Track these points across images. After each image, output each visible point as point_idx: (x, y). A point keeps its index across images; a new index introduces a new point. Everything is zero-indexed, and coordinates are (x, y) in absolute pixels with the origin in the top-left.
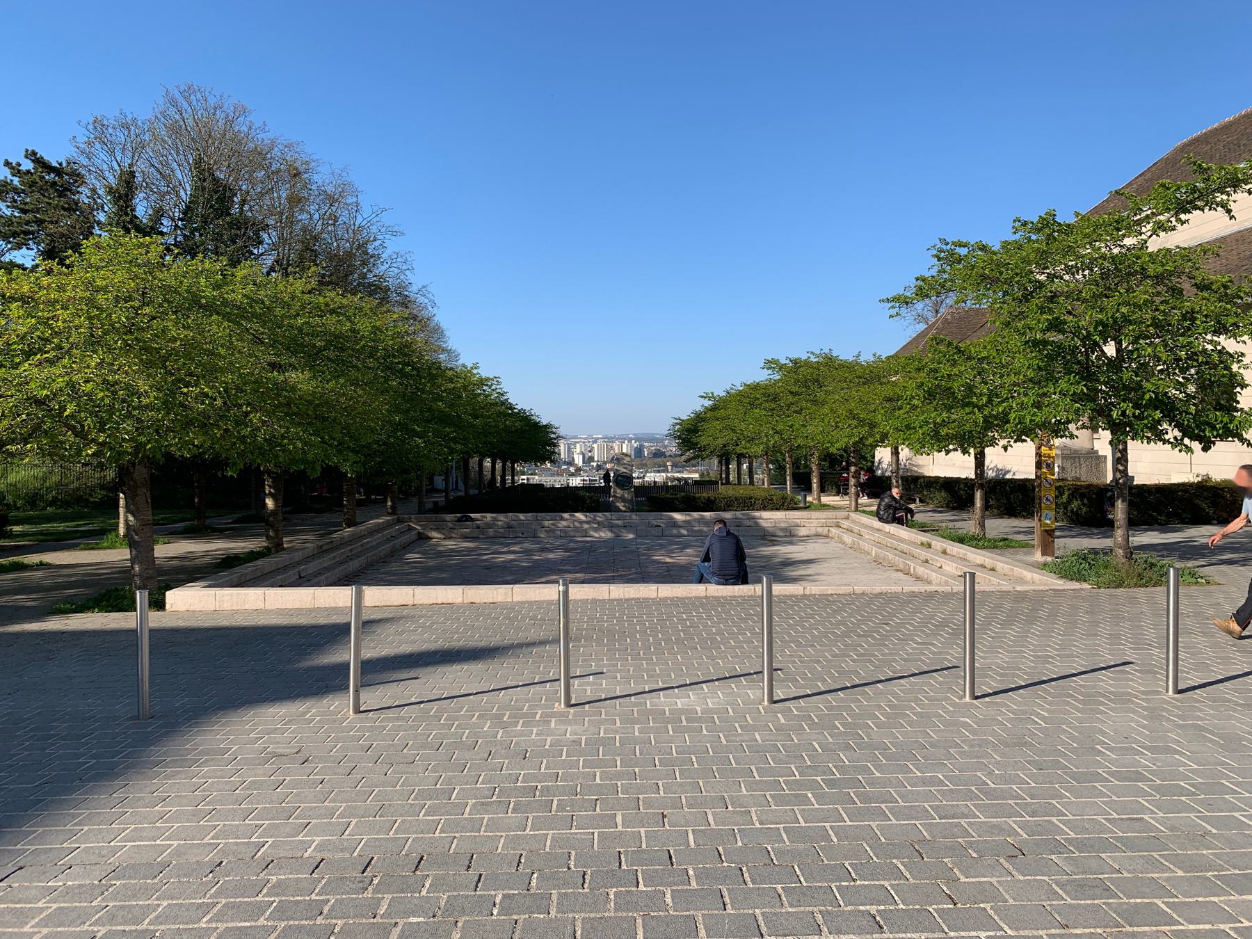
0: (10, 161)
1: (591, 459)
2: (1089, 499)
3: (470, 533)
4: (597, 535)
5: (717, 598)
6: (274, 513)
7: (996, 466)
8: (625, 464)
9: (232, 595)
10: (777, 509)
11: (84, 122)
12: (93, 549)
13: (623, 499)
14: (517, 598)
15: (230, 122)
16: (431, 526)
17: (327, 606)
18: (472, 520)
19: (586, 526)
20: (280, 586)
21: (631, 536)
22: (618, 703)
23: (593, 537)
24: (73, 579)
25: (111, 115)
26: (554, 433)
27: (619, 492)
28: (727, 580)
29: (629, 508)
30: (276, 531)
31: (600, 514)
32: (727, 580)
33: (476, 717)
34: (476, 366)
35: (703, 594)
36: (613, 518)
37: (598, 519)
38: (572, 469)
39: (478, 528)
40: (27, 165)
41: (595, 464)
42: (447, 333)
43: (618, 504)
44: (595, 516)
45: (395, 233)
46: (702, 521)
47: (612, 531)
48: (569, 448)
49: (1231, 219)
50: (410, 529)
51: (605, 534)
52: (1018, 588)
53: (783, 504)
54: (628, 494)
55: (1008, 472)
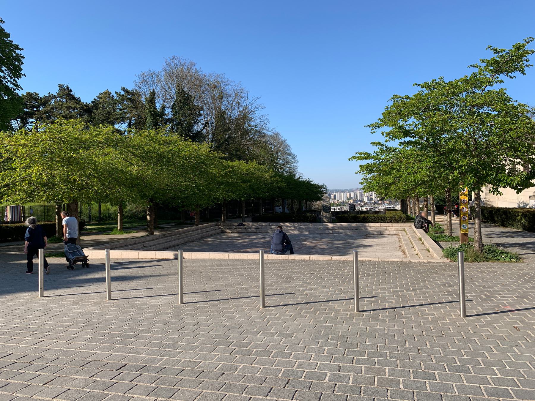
0: (117, 92)
1: (372, 199)
2: (529, 218)
3: (242, 230)
4: (293, 232)
5: (272, 260)
6: (150, 221)
7: (523, 201)
8: (327, 202)
9: (95, 252)
10: (397, 222)
11: (137, 75)
12: (108, 234)
13: (326, 217)
14: (193, 258)
15: (189, 69)
16: (228, 228)
17: (126, 258)
18: (244, 225)
19: (289, 228)
20: (131, 250)
21: (307, 233)
22: (387, 311)
23: (291, 233)
24: (248, 250)
25: (146, 70)
26: (324, 188)
27: (324, 214)
28: (277, 252)
29: (328, 221)
30: (151, 229)
31: (296, 223)
32: (277, 252)
33: (318, 313)
34: (357, 161)
35: (308, 259)
36: (302, 225)
37: (295, 225)
38: (362, 204)
39: (245, 228)
40: (123, 93)
41: (373, 201)
42: (291, 147)
43: (324, 219)
44: (294, 224)
45: (262, 108)
46: (342, 228)
47: (299, 231)
48: (361, 194)
49: (524, 75)
50: (220, 228)
51: (296, 232)
52: (412, 261)
53: (400, 220)
54: (328, 215)
55: (528, 204)
